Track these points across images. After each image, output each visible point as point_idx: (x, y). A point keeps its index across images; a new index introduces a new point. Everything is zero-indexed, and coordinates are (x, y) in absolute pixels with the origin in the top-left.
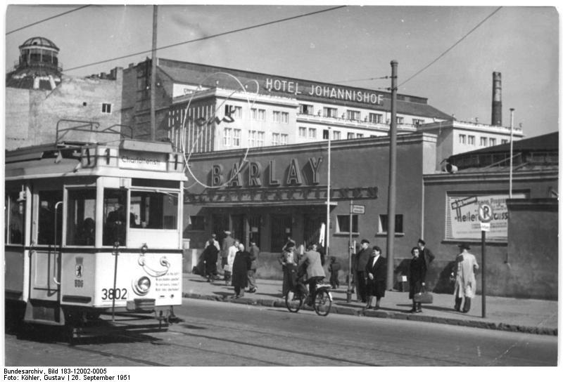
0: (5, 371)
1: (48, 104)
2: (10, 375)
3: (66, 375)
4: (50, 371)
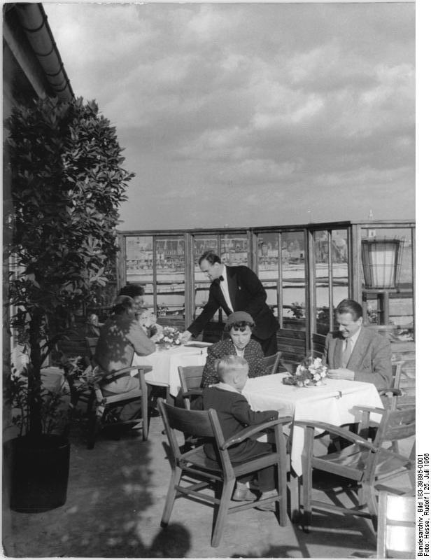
0: (420, 555)
1: (89, 272)
2: (424, 550)
3: (425, 495)
4: (420, 511)
